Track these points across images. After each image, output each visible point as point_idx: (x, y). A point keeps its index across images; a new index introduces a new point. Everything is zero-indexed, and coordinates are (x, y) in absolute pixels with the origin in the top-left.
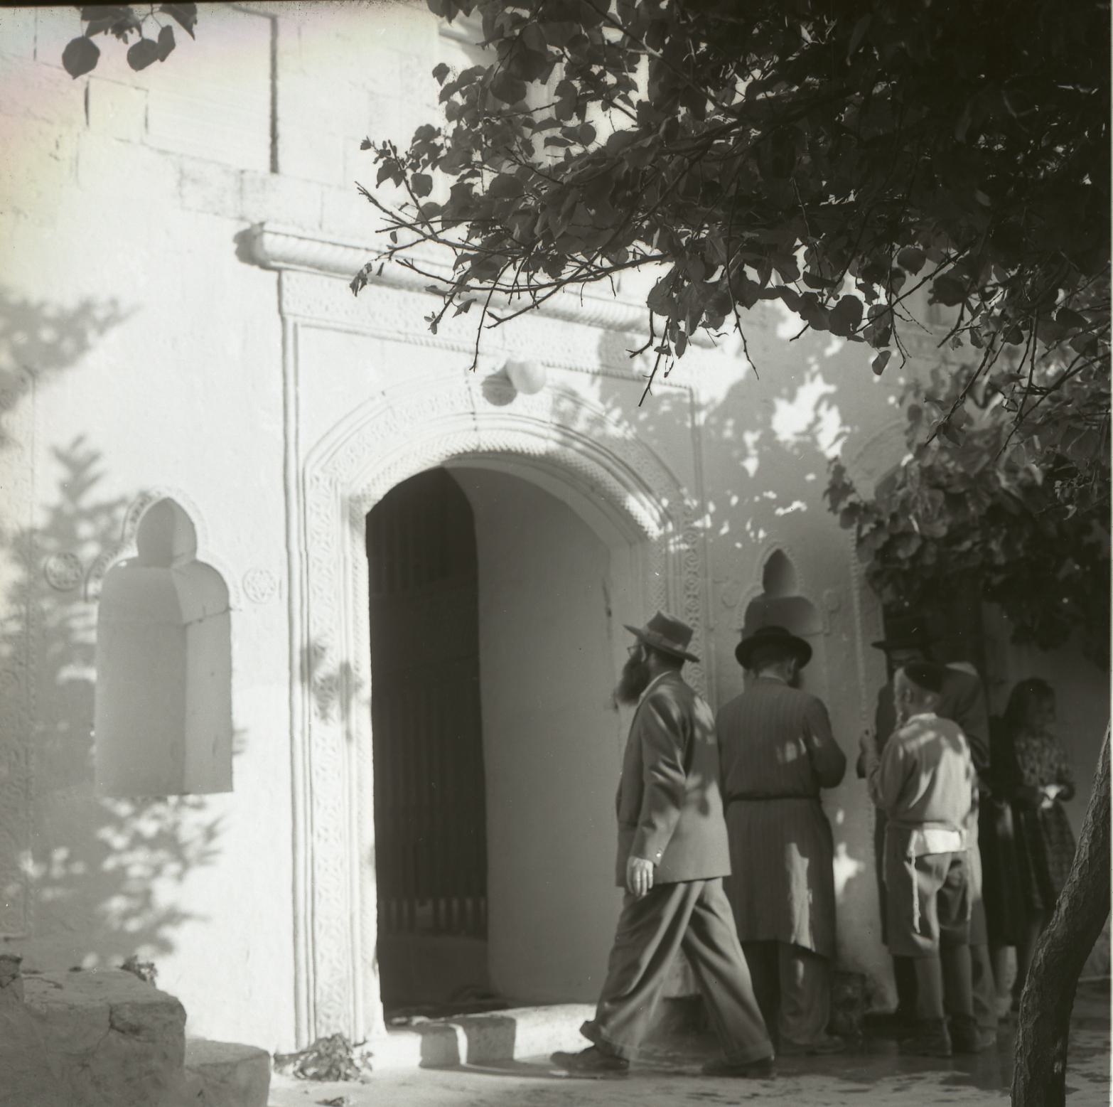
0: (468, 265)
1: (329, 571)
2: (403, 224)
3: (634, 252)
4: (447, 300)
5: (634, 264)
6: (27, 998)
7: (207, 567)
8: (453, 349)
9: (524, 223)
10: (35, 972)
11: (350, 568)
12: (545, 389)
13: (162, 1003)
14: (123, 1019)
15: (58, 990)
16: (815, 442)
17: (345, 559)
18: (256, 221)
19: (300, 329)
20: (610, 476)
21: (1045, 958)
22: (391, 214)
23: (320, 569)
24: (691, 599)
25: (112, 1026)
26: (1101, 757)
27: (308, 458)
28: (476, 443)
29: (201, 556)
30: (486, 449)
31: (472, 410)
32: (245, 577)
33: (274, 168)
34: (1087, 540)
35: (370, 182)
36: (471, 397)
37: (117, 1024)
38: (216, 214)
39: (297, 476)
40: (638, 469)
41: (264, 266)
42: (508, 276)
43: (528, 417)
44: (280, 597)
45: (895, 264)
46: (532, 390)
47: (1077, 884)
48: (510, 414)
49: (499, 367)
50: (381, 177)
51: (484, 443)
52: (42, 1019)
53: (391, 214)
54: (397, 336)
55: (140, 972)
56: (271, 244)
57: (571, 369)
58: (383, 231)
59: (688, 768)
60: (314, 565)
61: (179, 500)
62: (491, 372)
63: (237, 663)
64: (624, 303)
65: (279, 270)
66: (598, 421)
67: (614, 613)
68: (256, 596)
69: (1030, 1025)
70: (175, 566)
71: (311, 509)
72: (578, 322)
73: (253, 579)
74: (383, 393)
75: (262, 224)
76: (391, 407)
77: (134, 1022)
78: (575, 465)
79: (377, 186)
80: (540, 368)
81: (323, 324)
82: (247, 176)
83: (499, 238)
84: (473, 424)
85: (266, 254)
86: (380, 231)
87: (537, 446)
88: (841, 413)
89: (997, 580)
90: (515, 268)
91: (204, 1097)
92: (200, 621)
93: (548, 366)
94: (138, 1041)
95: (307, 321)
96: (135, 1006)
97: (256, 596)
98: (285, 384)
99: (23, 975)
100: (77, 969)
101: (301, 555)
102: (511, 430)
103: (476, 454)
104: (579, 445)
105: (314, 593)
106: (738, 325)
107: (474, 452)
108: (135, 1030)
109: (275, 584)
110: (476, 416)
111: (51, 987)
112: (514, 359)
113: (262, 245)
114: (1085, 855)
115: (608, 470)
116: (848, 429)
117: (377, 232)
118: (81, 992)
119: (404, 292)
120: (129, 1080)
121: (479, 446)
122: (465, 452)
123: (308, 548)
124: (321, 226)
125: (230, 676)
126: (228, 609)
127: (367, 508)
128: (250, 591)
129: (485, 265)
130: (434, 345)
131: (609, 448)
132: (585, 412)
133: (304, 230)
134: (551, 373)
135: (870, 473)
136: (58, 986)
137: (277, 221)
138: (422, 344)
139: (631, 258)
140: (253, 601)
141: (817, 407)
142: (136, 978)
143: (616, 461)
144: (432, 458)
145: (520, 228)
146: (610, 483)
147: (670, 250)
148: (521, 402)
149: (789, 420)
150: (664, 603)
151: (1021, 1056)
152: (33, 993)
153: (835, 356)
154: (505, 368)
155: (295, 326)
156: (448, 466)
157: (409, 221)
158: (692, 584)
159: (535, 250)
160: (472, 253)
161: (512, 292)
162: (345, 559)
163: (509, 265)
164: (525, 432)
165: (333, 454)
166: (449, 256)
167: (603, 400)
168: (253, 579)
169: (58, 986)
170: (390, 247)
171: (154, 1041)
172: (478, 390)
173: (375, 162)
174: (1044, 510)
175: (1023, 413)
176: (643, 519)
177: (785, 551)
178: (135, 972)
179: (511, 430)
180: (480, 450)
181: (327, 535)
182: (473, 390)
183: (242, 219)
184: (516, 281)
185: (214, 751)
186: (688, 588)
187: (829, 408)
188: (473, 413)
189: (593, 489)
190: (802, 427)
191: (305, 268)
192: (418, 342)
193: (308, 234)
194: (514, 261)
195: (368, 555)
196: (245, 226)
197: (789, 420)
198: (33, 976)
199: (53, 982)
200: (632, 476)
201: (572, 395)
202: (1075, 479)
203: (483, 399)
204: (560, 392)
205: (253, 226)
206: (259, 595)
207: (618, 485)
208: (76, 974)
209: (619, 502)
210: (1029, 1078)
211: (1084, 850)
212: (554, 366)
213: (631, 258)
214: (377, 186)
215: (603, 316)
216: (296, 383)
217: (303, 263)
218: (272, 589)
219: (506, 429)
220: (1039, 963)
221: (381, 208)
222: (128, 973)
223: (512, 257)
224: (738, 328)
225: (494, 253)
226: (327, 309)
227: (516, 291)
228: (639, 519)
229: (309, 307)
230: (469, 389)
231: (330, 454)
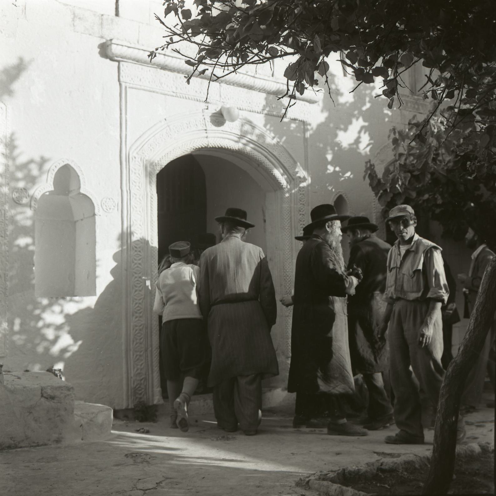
0: (203, 53)
1: (140, 199)
2: (175, 34)
3: (281, 51)
4: (195, 68)
5: (281, 56)
6: (5, 383)
7: (83, 194)
8: (197, 101)
9: (230, 37)
10: (9, 372)
11: (149, 198)
12: (239, 120)
13: (64, 386)
14: (47, 393)
15: (19, 380)
16: (358, 148)
17: (147, 194)
18: (109, 39)
19: (128, 89)
20: (267, 160)
21: (452, 371)
22: (170, 29)
23: (136, 198)
24: (301, 216)
25: (42, 396)
26: (481, 285)
27: (130, 148)
28: (207, 144)
29: (82, 191)
30: (211, 147)
31: (205, 129)
32: (102, 201)
33: (117, 14)
34: (477, 193)
35: (162, 15)
36: (205, 122)
37: (45, 395)
38: (90, 35)
39: (126, 156)
40: (279, 157)
41: (112, 59)
42: (223, 59)
43: (230, 133)
44: (118, 210)
45: (399, 60)
46: (232, 120)
47: (468, 340)
48: (222, 131)
49: (218, 110)
50: (167, 12)
51: (211, 144)
52: (12, 392)
53: (170, 29)
54: (172, 94)
55: (55, 373)
56: (115, 49)
57: (250, 111)
58: (167, 36)
59: (288, 343)
60: (133, 196)
61: (72, 165)
62: (214, 112)
63: (98, 239)
64: (275, 82)
65: (119, 62)
66: (261, 136)
67: (267, 221)
68: (107, 209)
69: (443, 400)
70: (71, 195)
71: (132, 171)
72: (254, 90)
73: (106, 202)
74: (165, 119)
75: (111, 40)
76: (169, 126)
77: (52, 394)
78: (251, 155)
79: (165, 17)
80: (237, 110)
81: (139, 87)
82: (104, 17)
83: (219, 42)
84: (206, 135)
85: (113, 54)
86: (165, 37)
87: (236, 146)
88: (370, 134)
89: (438, 211)
90: (226, 55)
91: (83, 427)
92: (82, 220)
93: (240, 109)
94: (54, 402)
95: (131, 85)
96: (53, 388)
97: (107, 209)
98: (121, 114)
99: (4, 373)
100: (27, 371)
101: (127, 192)
102: (223, 138)
103: (206, 149)
104: (252, 145)
105: (133, 208)
106: (327, 81)
107: (206, 147)
108: (52, 398)
109: (115, 204)
110: (207, 131)
111: (16, 378)
112: (225, 106)
113: (111, 49)
114: (472, 327)
115: (266, 157)
116: (372, 142)
117: (163, 37)
118: (29, 381)
119: (176, 74)
120: (50, 419)
121: (208, 145)
122: (202, 148)
123: (131, 189)
124: (138, 42)
125: (95, 245)
126: (94, 215)
127: (158, 170)
128: (104, 207)
129: (213, 52)
130: (189, 99)
131: (266, 147)
132: (257, 131)
133: (131, 44)
134: (241, 112)
135: (382, 161)
136: (19, 378)
137: (118, 39)
138: (183, 98)
139: (279, 54)
140: (106, 212)
141: (360, 132)
142: (53, 375)
143: (269, 153)
144: (187, 150)
145: (229, 36)
146: (266, 163)
147: (298, 48)
148: (228, 126)
149: (345, 138)
150: (289, 221)
151: (439, 413)
152: (8, 381)
153: (367, 110)
154: (221, 109)
155: (126, 87)
156: (194, 154)
157: (179, 32)
158: (302, 209)
159: (236, 48)
160: (207, 47)
161: (225, 66)
162: (147, 194)
163: (223, 54)
164: (229, 139)
165: (143, 146)
166: (196, 48)
167: (265, 126)
168: (106, 202)
169: (19, 378)
170: (167, 42)
171: (61, 403)
172: (208, 119)
173: (164, 5)
174: (462, 175)
175: (455, 124)
176: (281, 180)
177: (344, 195)
178: (52, 372)
179: (223, 138)
180: (209, 147)
181: (139, 183)
182: (206, 119)
183: (102, 37)
184: (227, 62)
185: (88, 278)
186: (300, 211)
187: (365, 133)
188: (206, 130)
189: (259, 165)
190: (352, 141)
191: (131, 61)
192: (182, 97)
193: (132, 46)
194: (226, 52)
195: (157, 193)
196: (104, 41)
197: (345, 138)
198: (8, 373)
199: (17, 376)
200: (277, 160)
201: (250, 123)
202: (476, 161)
203: (210, 124)
204: (244, 121)
205: (107, 41)
206: (108, 209)
207: (270, 164)
208: (26, 373)
209: (270, 171)
210: (442, 422)
211: (471, 325)
212: (243, 110)
213: (279, 54)
214: (165, 17)
215: (266, 87)
216: (126, 114)
217: (129, 59)
218: (114, 206)
219: (221, 138)
220: (449, 373)
221: (166, 26)
222: (50, 373)
223: (225, 50)
224: (326, 83)
225: (217, 48)
226: (140, 80)
227: (226, 66)
228: (279, 180)
229: (132, 79)
230: (204, 119)
231: (141, 146)
